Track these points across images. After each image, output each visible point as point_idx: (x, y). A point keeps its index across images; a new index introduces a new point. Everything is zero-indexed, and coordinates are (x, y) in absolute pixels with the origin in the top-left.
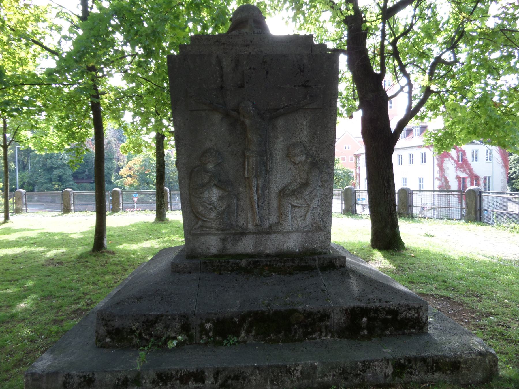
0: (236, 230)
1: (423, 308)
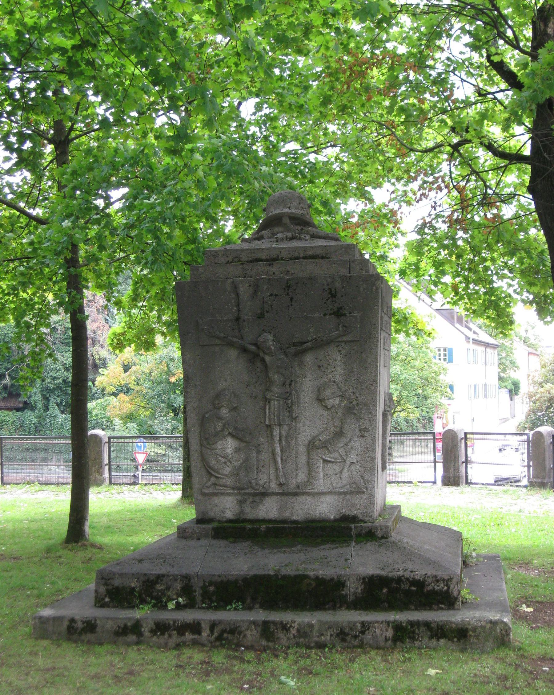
0: (256, 490)
1: (454, 581)
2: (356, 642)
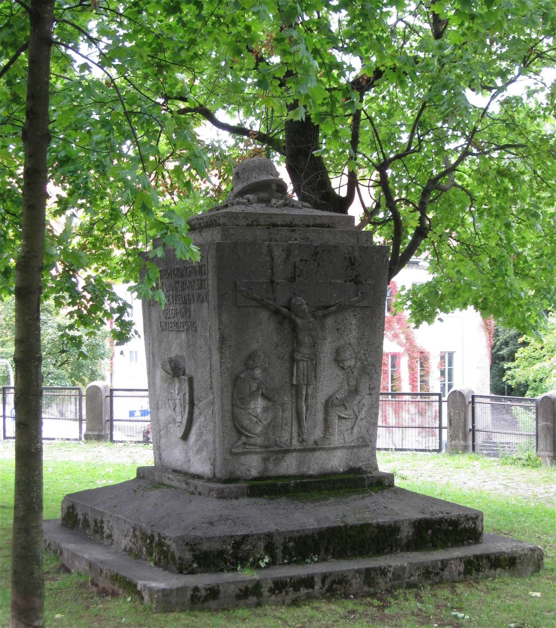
1: (480, 518)
2: (437, 579)
